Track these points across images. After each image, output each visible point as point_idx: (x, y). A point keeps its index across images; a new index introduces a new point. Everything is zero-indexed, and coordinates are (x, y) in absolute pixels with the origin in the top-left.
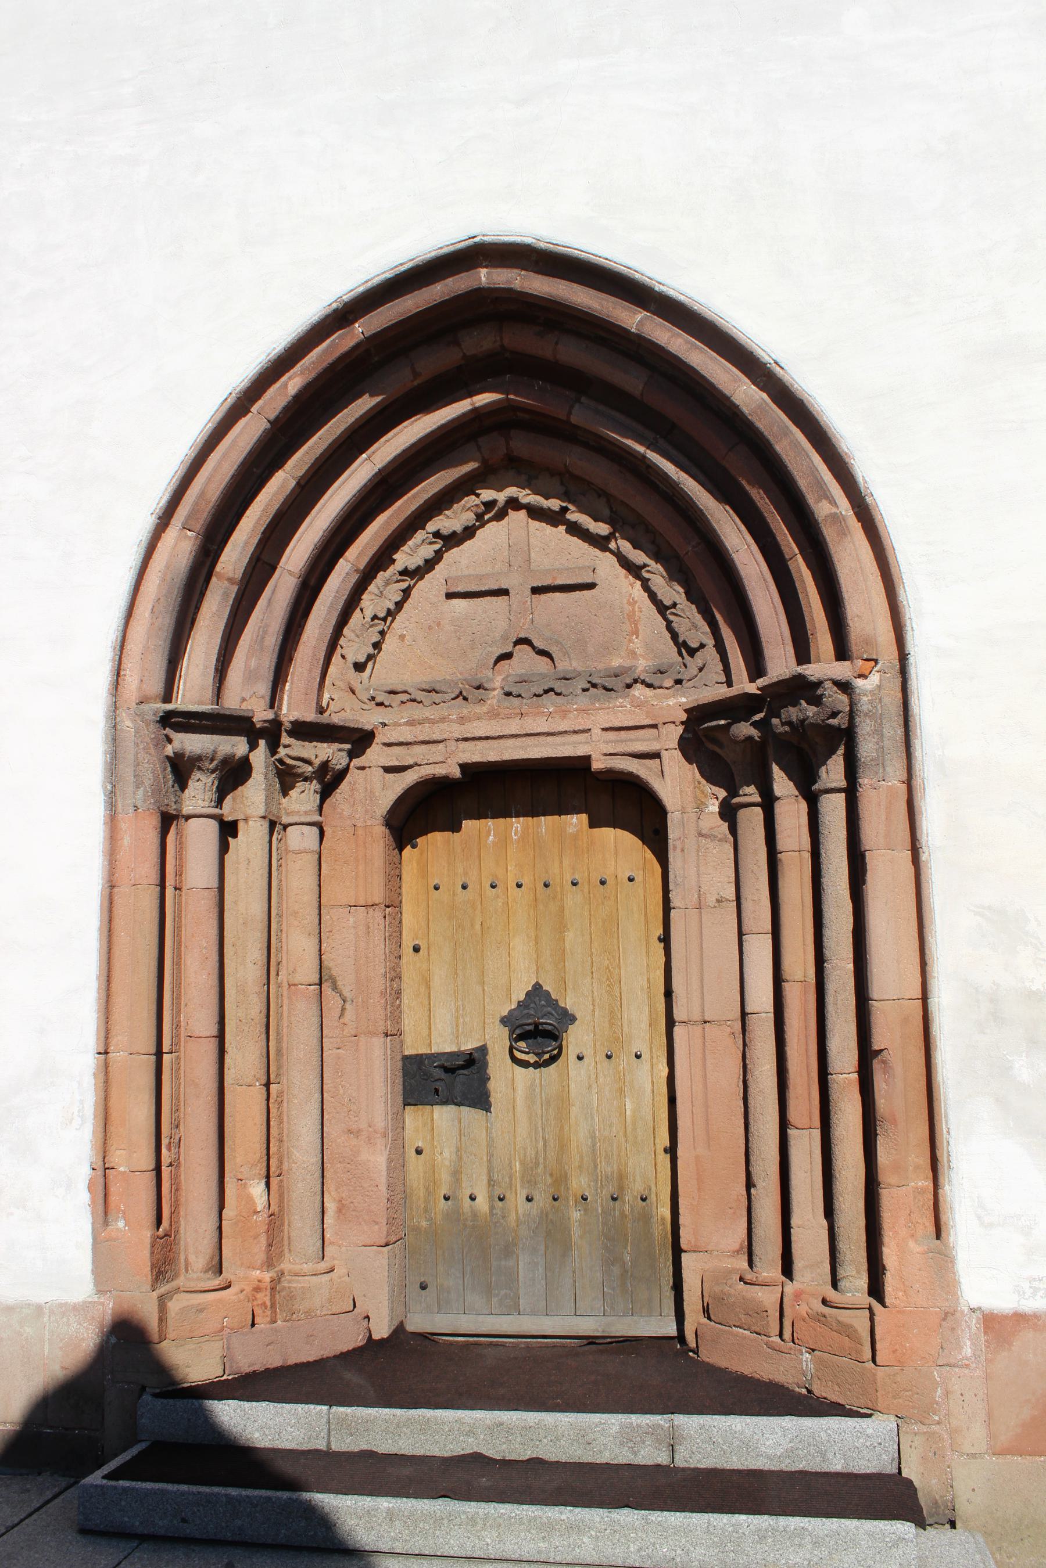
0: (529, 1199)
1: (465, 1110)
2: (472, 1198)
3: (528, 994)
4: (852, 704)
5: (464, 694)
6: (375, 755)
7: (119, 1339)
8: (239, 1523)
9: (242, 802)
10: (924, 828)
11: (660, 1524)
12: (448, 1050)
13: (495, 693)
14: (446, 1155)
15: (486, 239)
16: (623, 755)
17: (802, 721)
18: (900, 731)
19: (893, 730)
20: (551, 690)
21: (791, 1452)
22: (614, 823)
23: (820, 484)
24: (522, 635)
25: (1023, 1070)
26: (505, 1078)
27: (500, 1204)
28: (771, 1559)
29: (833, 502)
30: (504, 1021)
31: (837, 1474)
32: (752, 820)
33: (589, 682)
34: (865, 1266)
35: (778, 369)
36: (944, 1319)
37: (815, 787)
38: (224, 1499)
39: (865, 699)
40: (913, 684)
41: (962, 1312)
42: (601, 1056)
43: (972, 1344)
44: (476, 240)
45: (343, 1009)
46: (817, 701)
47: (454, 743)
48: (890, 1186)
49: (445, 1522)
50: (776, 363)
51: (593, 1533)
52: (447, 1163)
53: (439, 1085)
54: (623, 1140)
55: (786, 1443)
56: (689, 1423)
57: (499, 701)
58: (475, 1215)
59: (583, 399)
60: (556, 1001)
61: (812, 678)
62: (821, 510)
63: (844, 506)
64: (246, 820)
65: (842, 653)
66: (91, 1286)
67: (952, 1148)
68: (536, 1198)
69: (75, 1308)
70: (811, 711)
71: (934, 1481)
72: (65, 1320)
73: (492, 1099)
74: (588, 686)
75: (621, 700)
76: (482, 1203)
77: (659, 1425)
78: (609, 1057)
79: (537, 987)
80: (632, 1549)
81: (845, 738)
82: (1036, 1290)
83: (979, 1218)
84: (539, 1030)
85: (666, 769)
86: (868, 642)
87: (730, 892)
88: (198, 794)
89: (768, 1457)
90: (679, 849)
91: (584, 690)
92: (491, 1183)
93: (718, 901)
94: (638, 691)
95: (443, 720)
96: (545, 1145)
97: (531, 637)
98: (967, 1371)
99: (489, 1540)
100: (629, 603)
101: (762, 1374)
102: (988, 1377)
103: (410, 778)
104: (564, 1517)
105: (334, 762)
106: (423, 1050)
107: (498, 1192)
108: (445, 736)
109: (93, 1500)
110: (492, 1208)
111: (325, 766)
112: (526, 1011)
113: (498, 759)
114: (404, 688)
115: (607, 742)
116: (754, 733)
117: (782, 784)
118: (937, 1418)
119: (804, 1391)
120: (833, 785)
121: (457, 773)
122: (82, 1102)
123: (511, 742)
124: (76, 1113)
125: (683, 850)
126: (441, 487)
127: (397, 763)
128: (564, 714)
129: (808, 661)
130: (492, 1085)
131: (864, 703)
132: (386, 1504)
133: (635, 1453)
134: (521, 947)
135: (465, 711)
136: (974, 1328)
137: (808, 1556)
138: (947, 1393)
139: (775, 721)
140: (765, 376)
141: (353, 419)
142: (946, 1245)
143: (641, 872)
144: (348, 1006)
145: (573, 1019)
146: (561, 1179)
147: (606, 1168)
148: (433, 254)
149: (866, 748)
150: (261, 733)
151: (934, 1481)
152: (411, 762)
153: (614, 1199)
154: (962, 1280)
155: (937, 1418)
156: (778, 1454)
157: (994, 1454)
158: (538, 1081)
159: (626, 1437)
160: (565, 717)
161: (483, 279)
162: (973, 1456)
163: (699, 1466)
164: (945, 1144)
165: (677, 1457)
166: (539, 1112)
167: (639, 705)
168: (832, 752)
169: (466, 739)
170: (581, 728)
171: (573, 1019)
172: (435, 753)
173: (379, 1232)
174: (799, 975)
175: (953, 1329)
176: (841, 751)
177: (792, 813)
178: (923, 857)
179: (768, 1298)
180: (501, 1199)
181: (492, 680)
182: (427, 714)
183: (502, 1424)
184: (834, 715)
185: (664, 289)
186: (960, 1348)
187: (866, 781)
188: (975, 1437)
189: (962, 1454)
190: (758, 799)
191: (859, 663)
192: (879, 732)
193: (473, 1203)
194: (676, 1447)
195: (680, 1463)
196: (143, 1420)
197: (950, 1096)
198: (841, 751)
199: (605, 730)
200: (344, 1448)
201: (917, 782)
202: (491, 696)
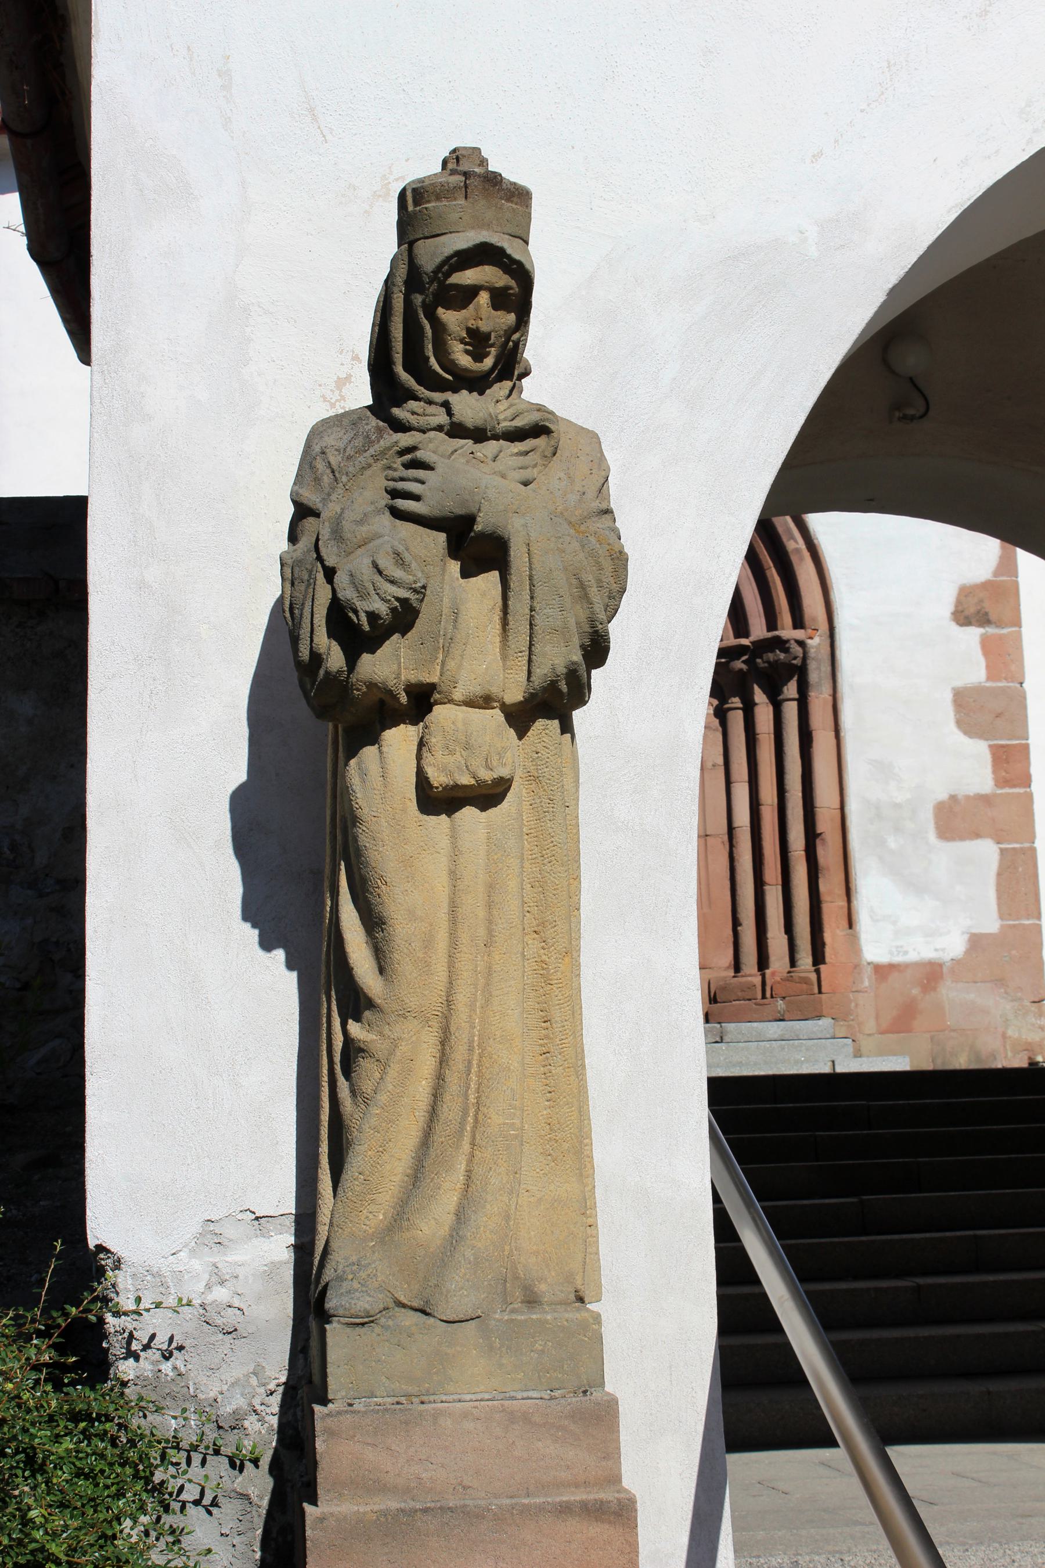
4: (805, 653)
17: (776, 661)
18: (829, 669)
19: (827, 668)
22: (753, 700)
23: (788, 530)
25: (892, 843)
29: (796, 542)
32: (737, 719)
34: (810, 952)
37: (781, 697)
40: (838, 643)
46: (786, 650)
62: (790, 546)
63: (801, 544)
65: (798, 622)
70: (782, 656)
81: (801, 672)
82: (899, 952)
83: (871, 917)
86: (814, 620)
87: (720, 760)
93: (714, 766)
116: (744, 667)
117: (759, 696)
120: (792, 697)
129: (776, 629)
131: (812, 652)
138: (857, 1005)
139: (759, 661)
149: (813, 676)
162: (869, 1035)
168: (791, 678)
174: (769, 802)
176: (795, 678)
177: (764, 714)
178: (842, 734)
184: (795, 658)
186: (862, 982)
188: (870, 1026)
190: (741, 706)
191: (810, 631)
192: (818, 668)
198: (795, 678)
201: (839, 695)
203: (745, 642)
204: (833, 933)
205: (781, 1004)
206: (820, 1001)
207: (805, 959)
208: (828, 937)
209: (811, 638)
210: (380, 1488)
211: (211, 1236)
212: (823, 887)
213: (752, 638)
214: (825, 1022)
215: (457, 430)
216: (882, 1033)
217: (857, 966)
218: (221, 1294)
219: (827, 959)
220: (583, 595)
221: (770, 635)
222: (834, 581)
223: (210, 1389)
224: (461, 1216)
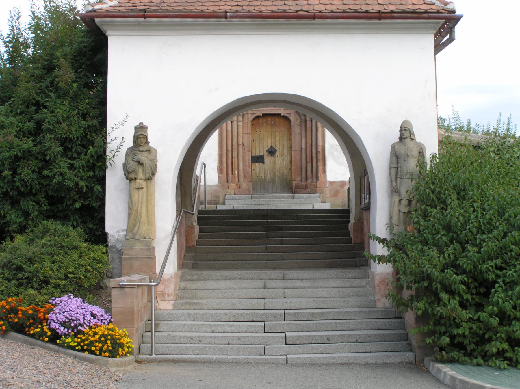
14: (258, 170)
25: (335, 154)
26: (268, 159)
76: (263, 177)
84: (272, 152)
92: (264, 174)
103: (255, 115)
126: (377, 223)
134: (269, 140)
140: (297, 187)
146: (274, 173)
147: (281, 172)
173: (249, 180)
188: (328, 195)
204: (320, 174)
205: (309, 190)
207: (315, 180)
208: (319, 175)
210: (129, 255)
211: (118, 231)
212: (319, 164)
215: (140, 151)
217: (326, 182)
218: (119, 237)
220: (151, 168)
223: (118, 247)
224: (138, 230)
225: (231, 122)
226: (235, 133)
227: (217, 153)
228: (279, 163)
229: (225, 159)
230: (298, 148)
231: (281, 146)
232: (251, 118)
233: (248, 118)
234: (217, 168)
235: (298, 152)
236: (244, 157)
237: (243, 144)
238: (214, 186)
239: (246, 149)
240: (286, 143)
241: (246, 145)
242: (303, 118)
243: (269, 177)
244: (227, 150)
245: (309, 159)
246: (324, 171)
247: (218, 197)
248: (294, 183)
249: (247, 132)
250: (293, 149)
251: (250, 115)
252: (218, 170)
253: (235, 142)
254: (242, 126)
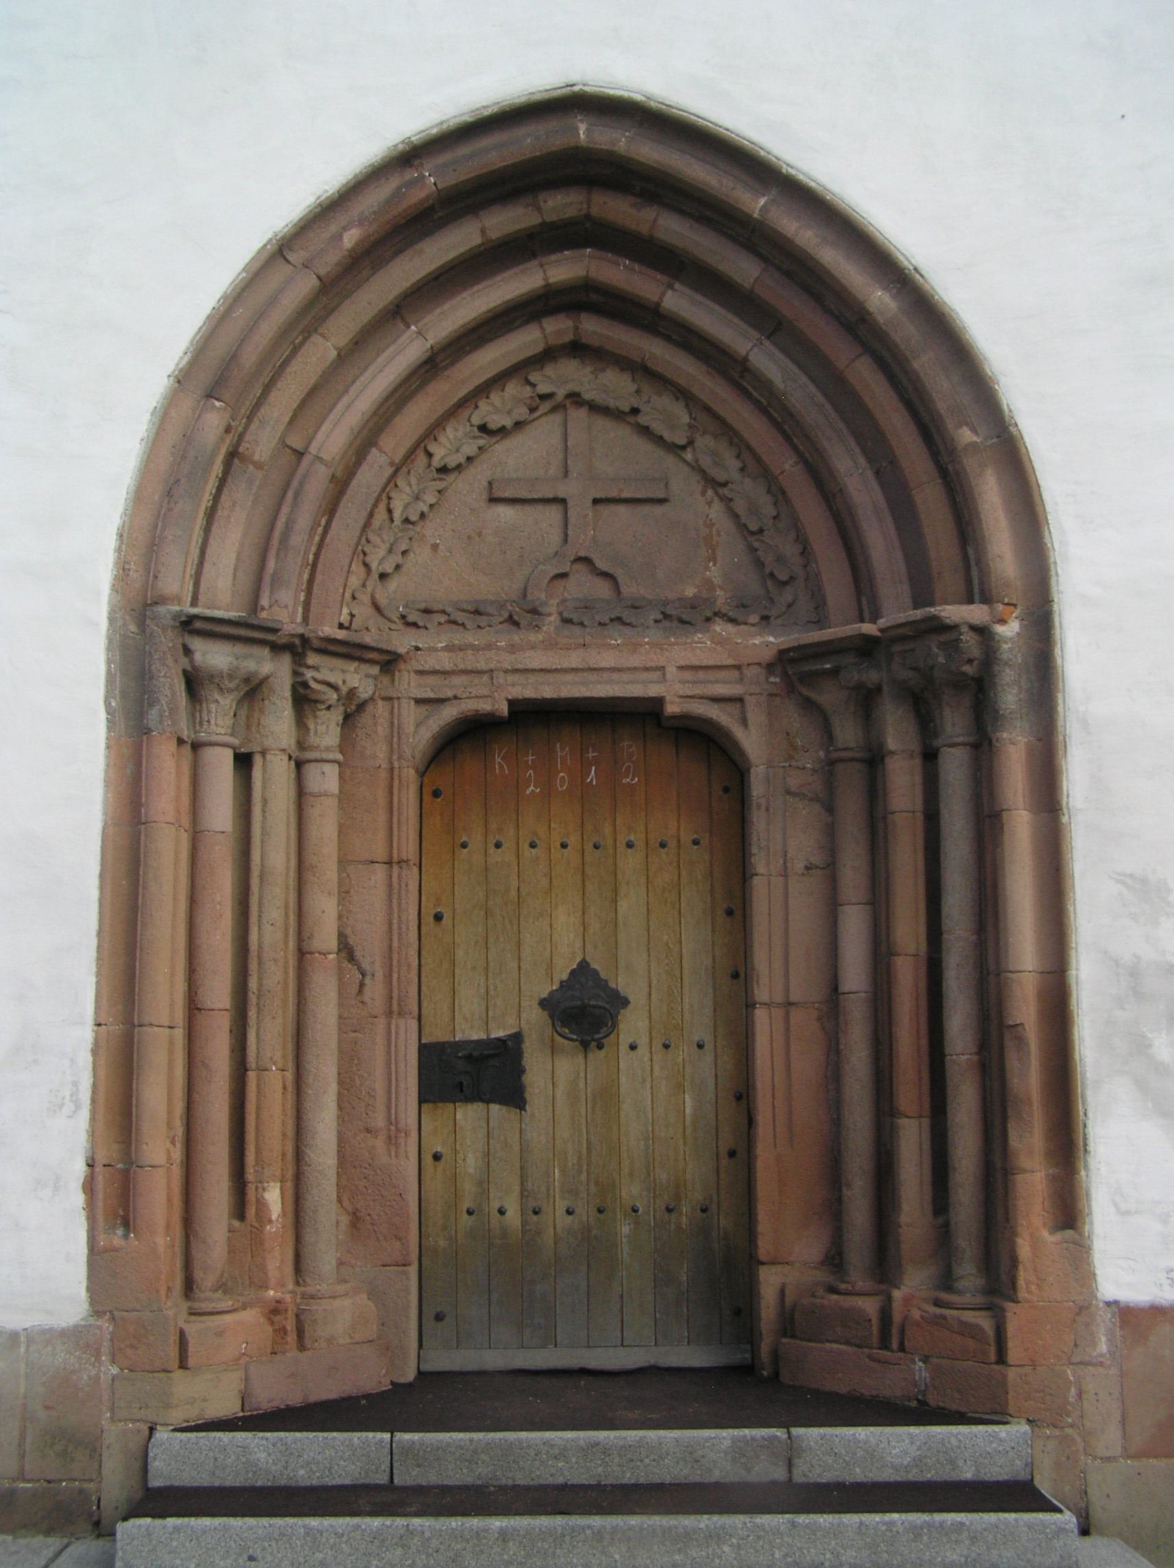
0: (569, 1212)
1: (495, 1108)
2: (502, 1212)
3: (573, 972)
5: (516, 617)
6: (408, 684)
7: (122, 1369)
8: (320, 1556)
9: (258, 732)
10: (1065, 788)
11: (807, 1526)
12: (475, 1037)
13: (552, 618)
14: (471, 1163)
15: (587, 89)
16: (702, 698)
20: (619, 619)
21: (918, 1462)
24: (582, 554)
26: (551, 1072)
27: (535, 1218)
28: (927, 1556)
30: (543, 1003)
31: (966, 1484)
33: (662, 613)
35: (918, 276)
36: (1078, 1314)
38: (302, 1531)
39: (1005, 646)
41: (1097, 1306)
42: (658, 1045)
43: (1109, 1340)
44: (576, 89)
45: (362, 985)
46: (953, 647)
47: (501, 674)
48: (1024, 1171)
49: (567, 1539)
50: (915, 269)
51: (734, 1541)
52: (471, 1170)
53: (466, 1080)
54: (681, 1143)
55: (913, 1452)
56: (810, 1435)
57: (556, 628)
58: (504, 1233)
59: (677, 286)
60: (606, 981)
61: (948, 621)
64: (263, 753)
66: (86, 1306)
67: (1091, 1131)
68: (578, 1211)
69: (64, 1334)
71: (1067, 1488)
72: (50, 1349)
73: (527, 1096)
74: (660, 617)
75: (700, 636)
76: (513, 1217)
77: (776, 1437)
78: (666, 1046)
79: (584, 965)
80: (777, 1556)
81: (979, 690)
83: (1115, 1205)
84: (585, 1012)
85: (750, 715)
88: (220, 718)
89: (895, 1468)
90: (763, 808)
91: (656, 621)
92: (524, 1195)
93: (807, 868)
94: (719, 627)
95: (489, 647)
96: (589, 1149)
97: (593, 556)
98: (1101, 1369)
99: (617, 1557)
100: (705, 524)
101: (863, 1391)
102: (1122, 1374)
103: (449, 714)
104: (702, 1525)
105: (361, 690)
106: (447, 1038)
107: (532, 1204)
108: (492, 666)
109: (135, 1542)
110: (524, 1223)
111: (352, 692)
112: (570, 993)
113: (555, 696)
114: (441, 607)
115: (683, 682)
118: (1070, 1420)
119: (914, 1404)
121: (504, 709)
122: (75, 1084)
123: (569, 677)
124: (68, 1097)
125: (767, 810)
127: (432, 695)
128: (635, 648)
130: (528, 1079)
132: (498, 1523)
133: (748, 1470)
134: (565, 921)
135: (516, 638)
136: (1108, 1323)
137: (965, 1552)
138: (1080, 1395)
141: (408, 284)
142: (1081, 1234)
143: (707, 835)
144: (368, 981)
145: (625, 1002)
147: (662, 1176)
148: (523, 99)
150: (288, 648)
151: (1067, 1488)
152: (450, 694)
153: (669, 1210)
154: (1097, 1272)
155: (1070, 1420)
156: (905, 1463)
157: (1129, 1457)
158: (582, 1075)
159: (739, 1451)
160: (635, 651)
161: (582, 136)
163: (819, 1480)
164: (1081, 1126)
165: (795, 1471)
166: (583, 1111)
167: (720, 641)
169: (516, 671)
170: (653, 664)
171: (625, 1002)
172: (480, 686)
175: (1087, 1325)
179: (870, 1306)
180: (536, 1213)
181: (544, 604)
182: (471, 639)
183: (598, 1444)
185: (792, 172)
186: (1094, 1343)
187: (1005, 735)
188: (1110, 1439)
189: (1095, 1458)
191: (1000, 607)
193: (502, 1218)
194: (795, 1461)
195: (798, 1477)
196: (157, 1463)
197: (1088, 1075)
199: (681, 668)
200: (410, 1482)
202: (546, 622)
203: (868, 628)
204: (1033, 1233)
206: (1003, 1383)
207: (969, 1275)
209: (1003, 621)
213: (882, 622)
214: (1018, 1429)
216: (1137, 1456)
217: (1084, 1308)
219: (1022, 1294)
221: (919, 614)
222: (1049, 508)
225: (243, 762)
226: (275, 853)
227: (85, 1034)
228: (636, 1107)
229: (159, 1095)
230: (805, 985)
231: (654, 952)
232: (420, 732)
233: (395, 730)
234: (79, 1168)
235: (805, 1022)
236: (349, 1060)
237: (347, 950)
238: (49, 1336)
239: (375, 992)
240: (696, 940)
241: (371, 952)
242: (848, 734)
243: (556, 1220)
244: (193, 1007)
245: (910, 1090)
246: (1068, 1211)
247: (75, 1442)
248: (770, 1282)
249: (380, 852)
250: (761, 993)
251: (409, 714)
252: (89, 1187)
253: (272, 929)
254: (345, 798)
